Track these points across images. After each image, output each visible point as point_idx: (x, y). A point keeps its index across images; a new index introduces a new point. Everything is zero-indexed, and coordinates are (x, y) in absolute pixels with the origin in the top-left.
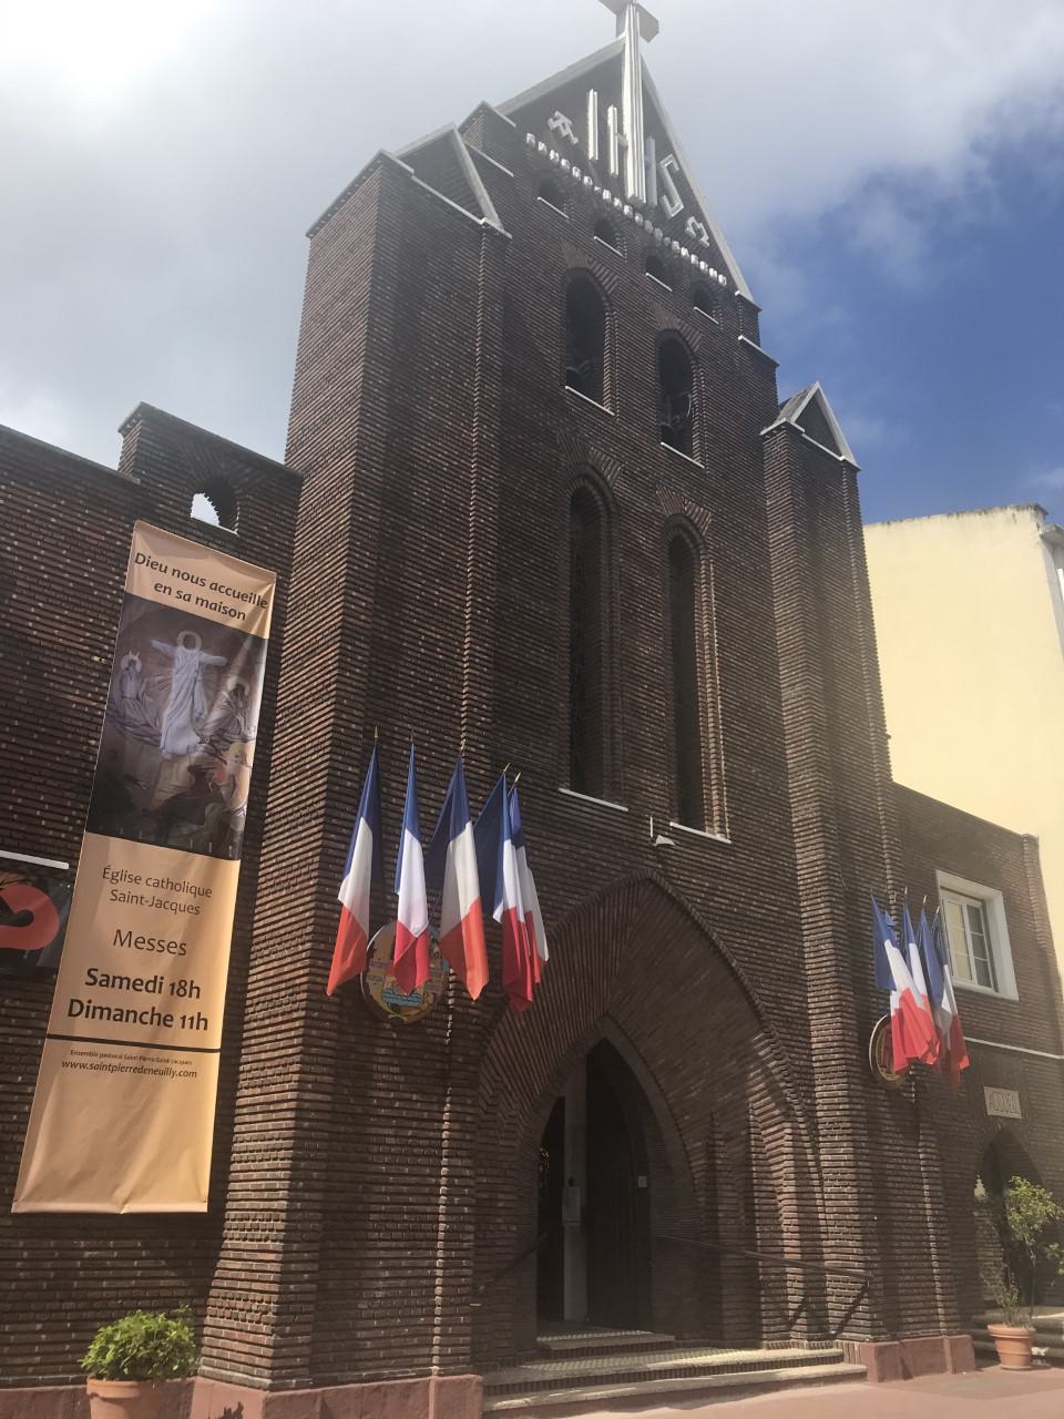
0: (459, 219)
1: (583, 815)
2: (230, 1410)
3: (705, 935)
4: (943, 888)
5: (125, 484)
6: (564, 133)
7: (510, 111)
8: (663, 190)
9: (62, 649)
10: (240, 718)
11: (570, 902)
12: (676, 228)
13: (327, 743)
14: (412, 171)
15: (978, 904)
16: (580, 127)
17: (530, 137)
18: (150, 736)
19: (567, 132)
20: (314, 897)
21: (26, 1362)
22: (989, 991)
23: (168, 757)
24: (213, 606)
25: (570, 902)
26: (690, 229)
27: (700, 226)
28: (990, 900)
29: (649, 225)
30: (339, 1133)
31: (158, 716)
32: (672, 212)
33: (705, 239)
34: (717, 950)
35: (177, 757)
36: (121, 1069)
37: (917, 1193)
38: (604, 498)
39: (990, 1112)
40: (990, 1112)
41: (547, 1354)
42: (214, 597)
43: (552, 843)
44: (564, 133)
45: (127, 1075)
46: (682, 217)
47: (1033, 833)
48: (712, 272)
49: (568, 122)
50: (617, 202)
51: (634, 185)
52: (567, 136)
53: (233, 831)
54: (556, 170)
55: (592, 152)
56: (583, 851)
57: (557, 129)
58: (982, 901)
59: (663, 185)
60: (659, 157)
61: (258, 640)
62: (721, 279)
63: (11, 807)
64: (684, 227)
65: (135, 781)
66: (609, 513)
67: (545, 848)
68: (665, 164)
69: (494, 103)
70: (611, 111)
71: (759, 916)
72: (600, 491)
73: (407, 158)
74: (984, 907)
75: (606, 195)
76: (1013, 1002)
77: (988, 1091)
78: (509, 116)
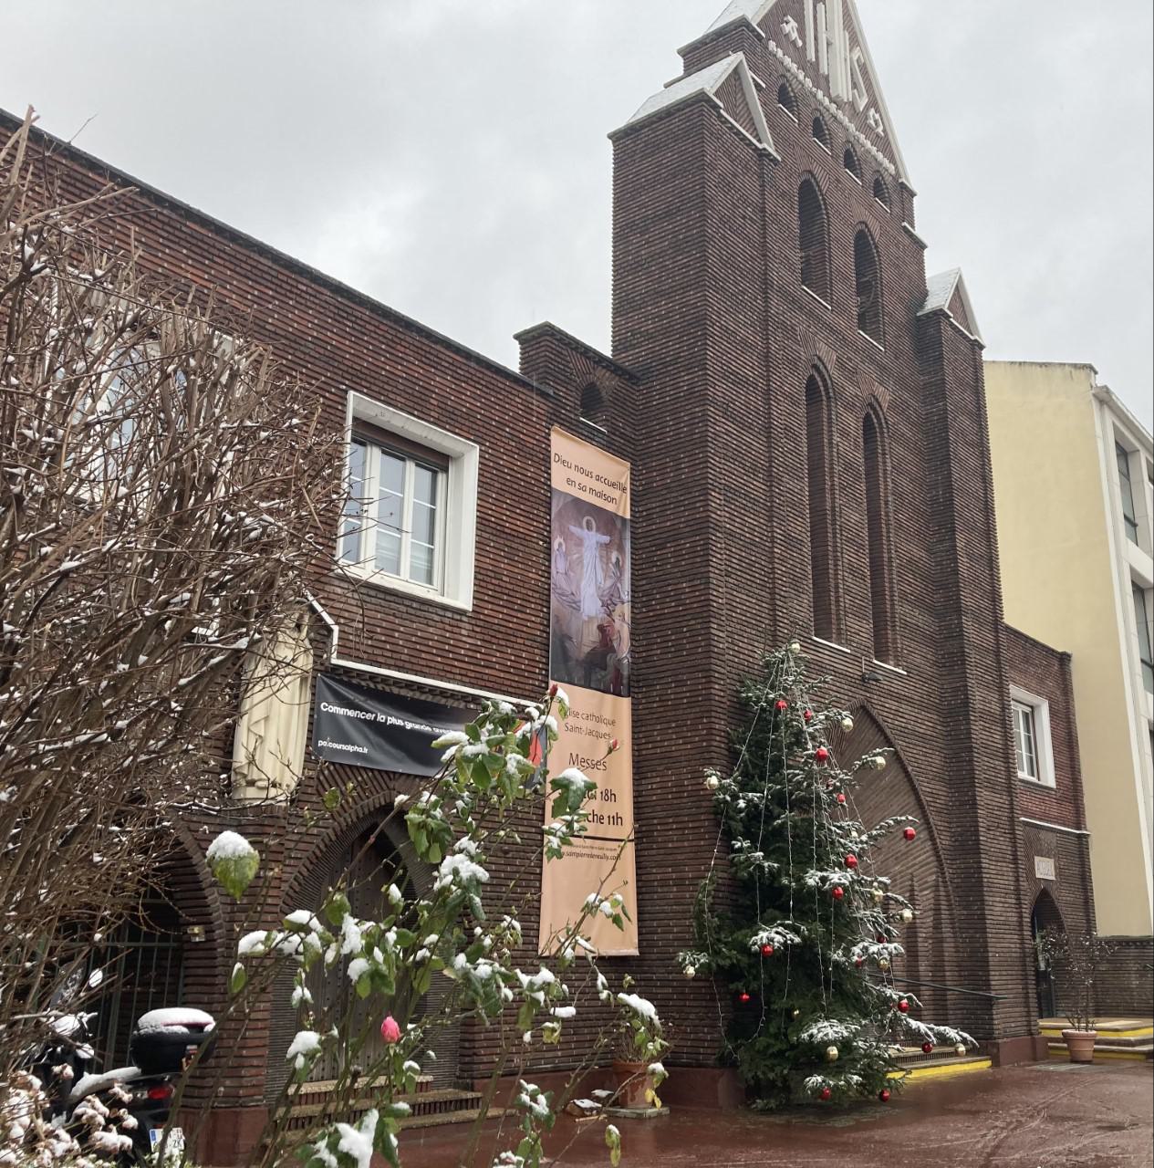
0: (771, 160)
9: (523, 536)
10: (619, 585)
14: (722, 105)
15: (1028, 710)
18: (575, 603)
22: (1034, 779)
23: (586, 619)
24: (600, 495)
28: (1039, 706)
31: (578, 587)
33: (880, 130)
35: (591, 618)
36: (582, 855)
37: (192, 886)
38: (825, 385)
39: (1038, 876)
40: (1038, 876)
42: (599, 486)
45: (585, 858)
47: (1069, 652)
53: (622, 675)
55: (811, 55)
58: (1032, 707)
61: (624, 520)
65: (570, 638)
66: (829, 398)
71: (496, 621)
72: (824, 380)
74: (1033, 712)
76: (1051, 789)
77: (1037, 859)
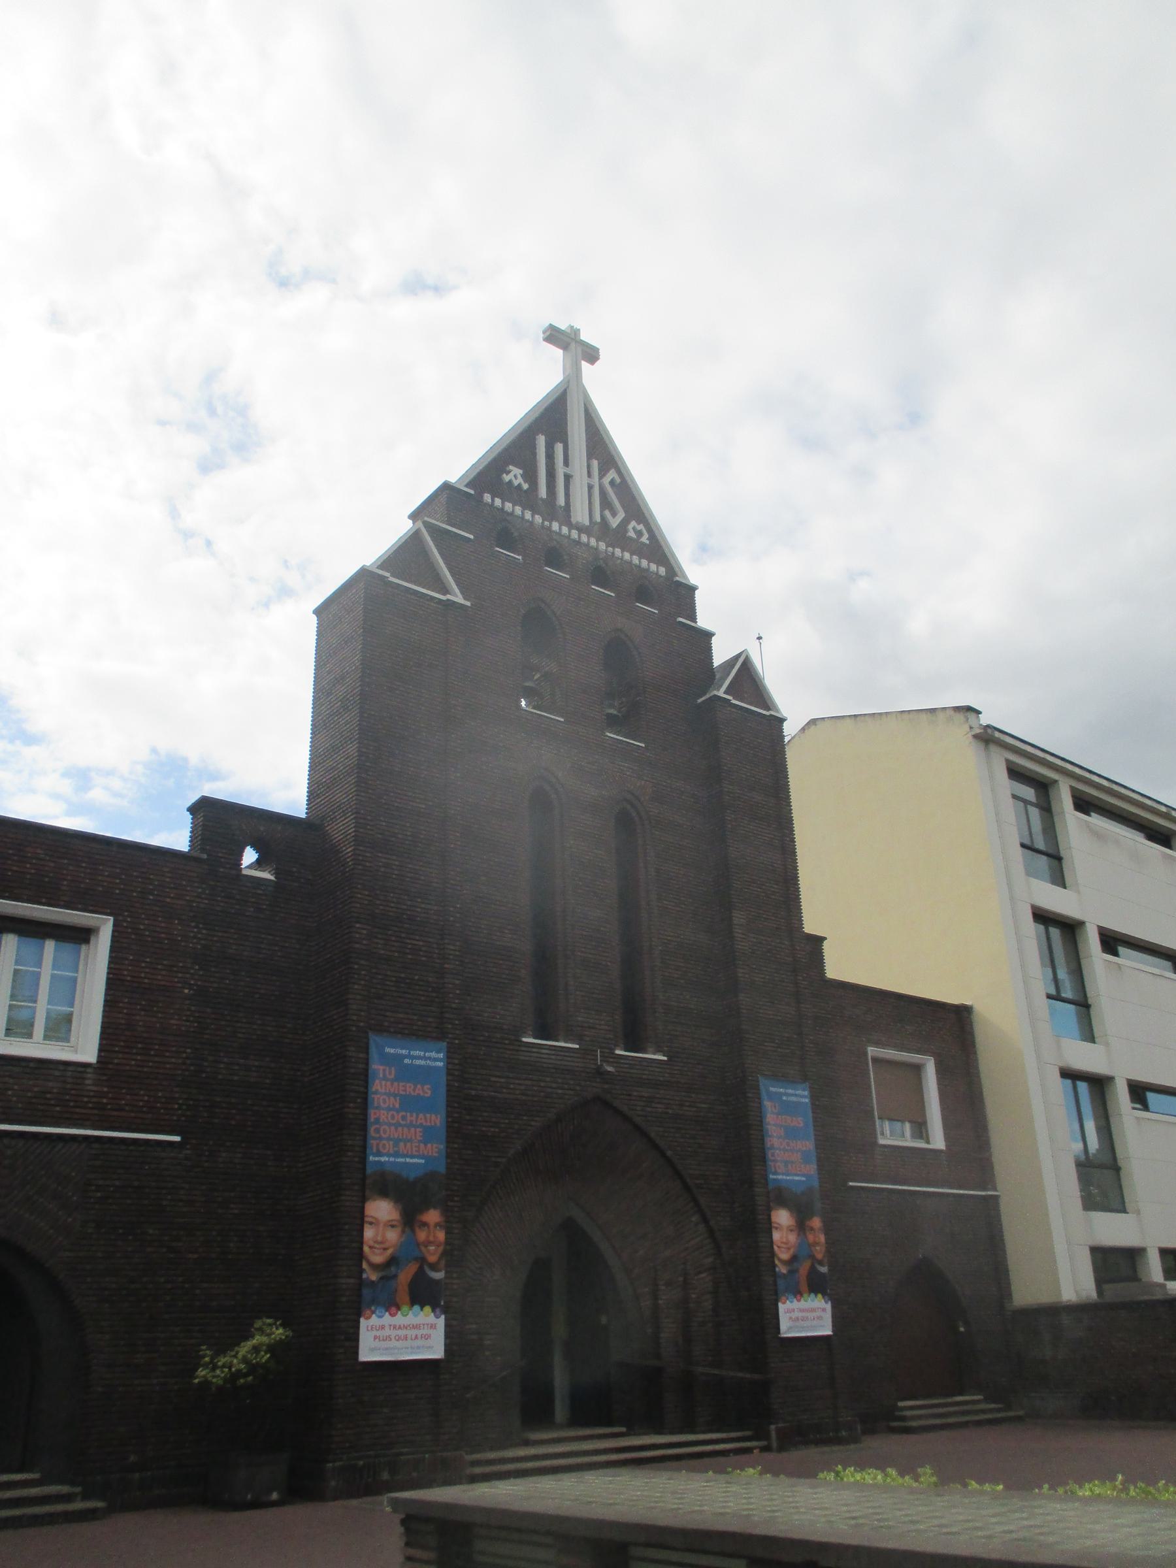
1: (542, 1056)
2: (573, 327)
3: (644, 1134)
4: (1111, 942)
5: (197, 860)
6: (516, 483)
7: (465, 483)
8: (606, 503)
11: (533, 1123)
12: (618, 537)
13: (352, 826)
16: (530, 475)
17: (487, 498)
19: (519, 481)
20: (355, 784)
21: (1158, 805)
22: (921, 1145)
25: (533, 1123)
26: (632, 534)
27: (641, 527)
29: (593, 542)
30: (585, 948)
32: (614, 522)
33: (645, 539)
34: (655, 1146)
41: (527, 1443)
43: (517, 1082)
44: (516, 483)
46: (624, 524)
48: (653, 567)
49: (518, 472)
50: (565, 530)
51: (580, 514)
52: (520, 485)
54: (509, 518)
56: (542, 1084)
57: (510, 481)
59: (606, 498)
60: (603, 473)
62: (662, 571)
63: (141, 1104)
64: (626, 531)
67: (512, 1086)
68: (606, 480)
69: (453, 479)
70: (559, 448)
73: (381, 567)
75: (555, 526)
78: (467, 486)
